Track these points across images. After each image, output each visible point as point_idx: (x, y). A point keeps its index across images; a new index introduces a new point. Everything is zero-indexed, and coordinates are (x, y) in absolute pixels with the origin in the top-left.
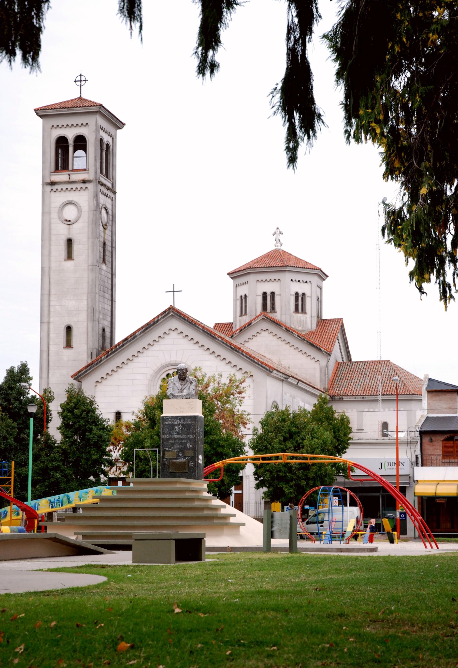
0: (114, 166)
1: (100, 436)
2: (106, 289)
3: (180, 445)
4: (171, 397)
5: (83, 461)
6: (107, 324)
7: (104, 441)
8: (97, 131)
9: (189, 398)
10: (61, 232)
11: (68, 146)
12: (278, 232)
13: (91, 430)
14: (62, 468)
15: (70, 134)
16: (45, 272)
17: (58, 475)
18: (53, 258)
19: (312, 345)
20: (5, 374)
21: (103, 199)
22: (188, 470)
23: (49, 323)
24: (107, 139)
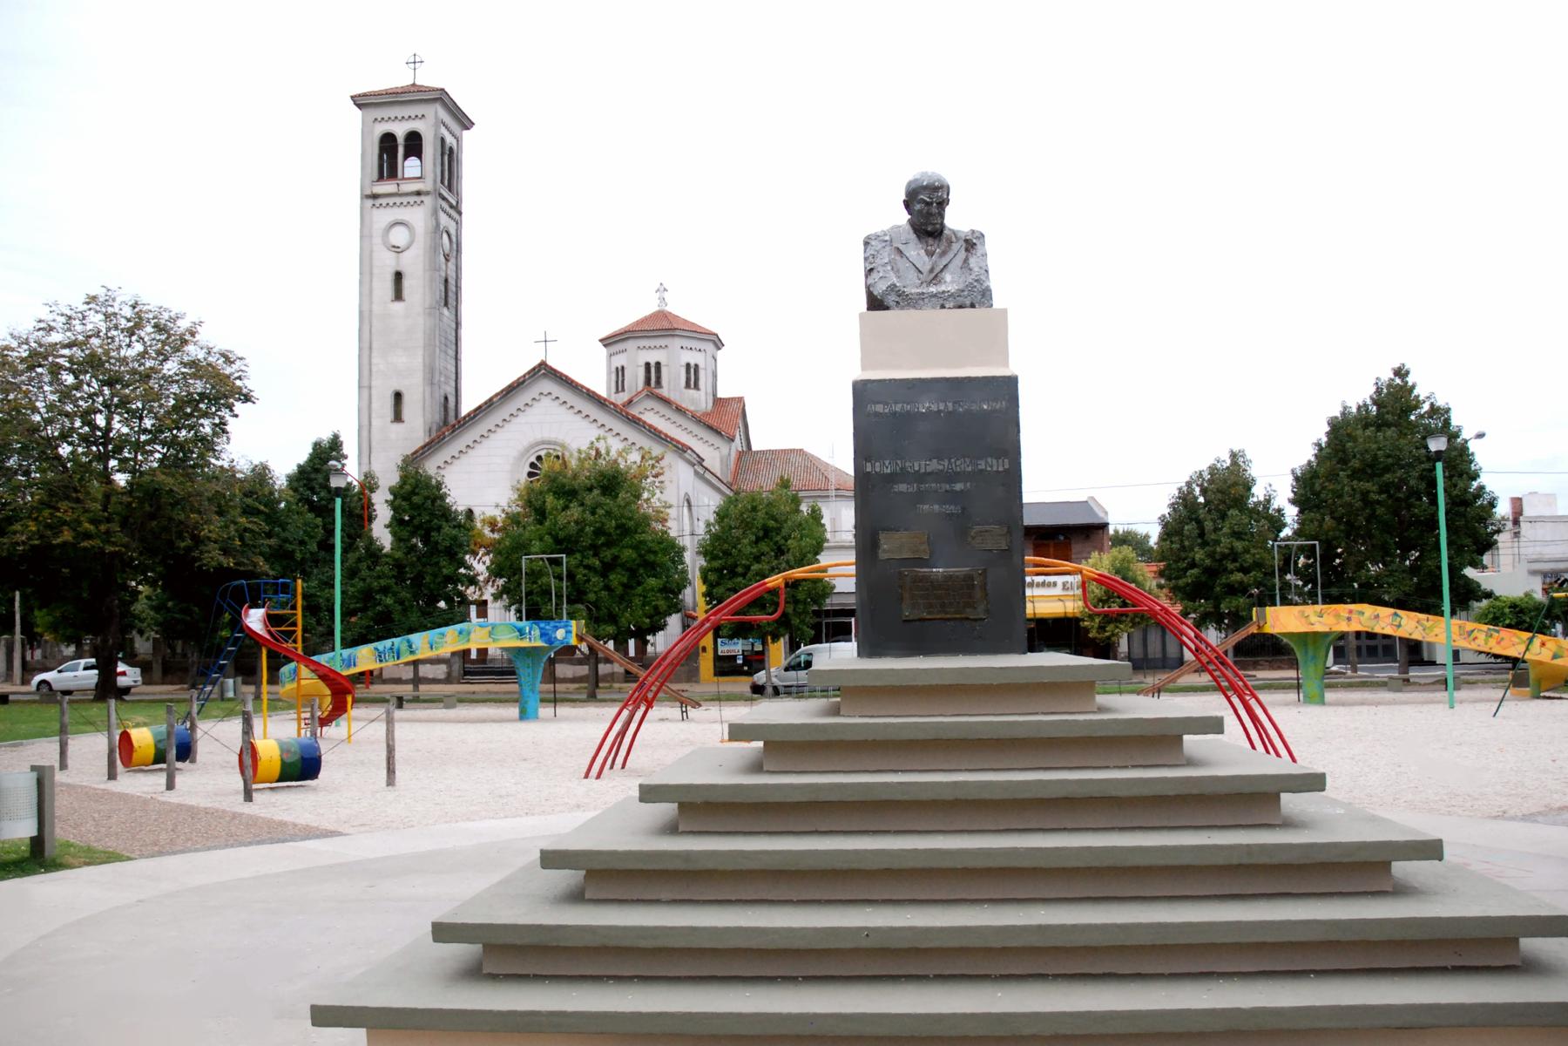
1: (455, 538)
2: (447, 342)
4: (891, 299)
5: (428, 579)
6: (450, 390)
7: (461, 546)
9: (973, 306)
10: (387, 263)
11: (396, 147)
13: (439, 529)
14: (395, 588)
15: (400, 131)
16: (365, 317)
17: (389, 601)
19: (710, 428)
22: (987, 611)
23: (370, 388)
24: (450, 140)
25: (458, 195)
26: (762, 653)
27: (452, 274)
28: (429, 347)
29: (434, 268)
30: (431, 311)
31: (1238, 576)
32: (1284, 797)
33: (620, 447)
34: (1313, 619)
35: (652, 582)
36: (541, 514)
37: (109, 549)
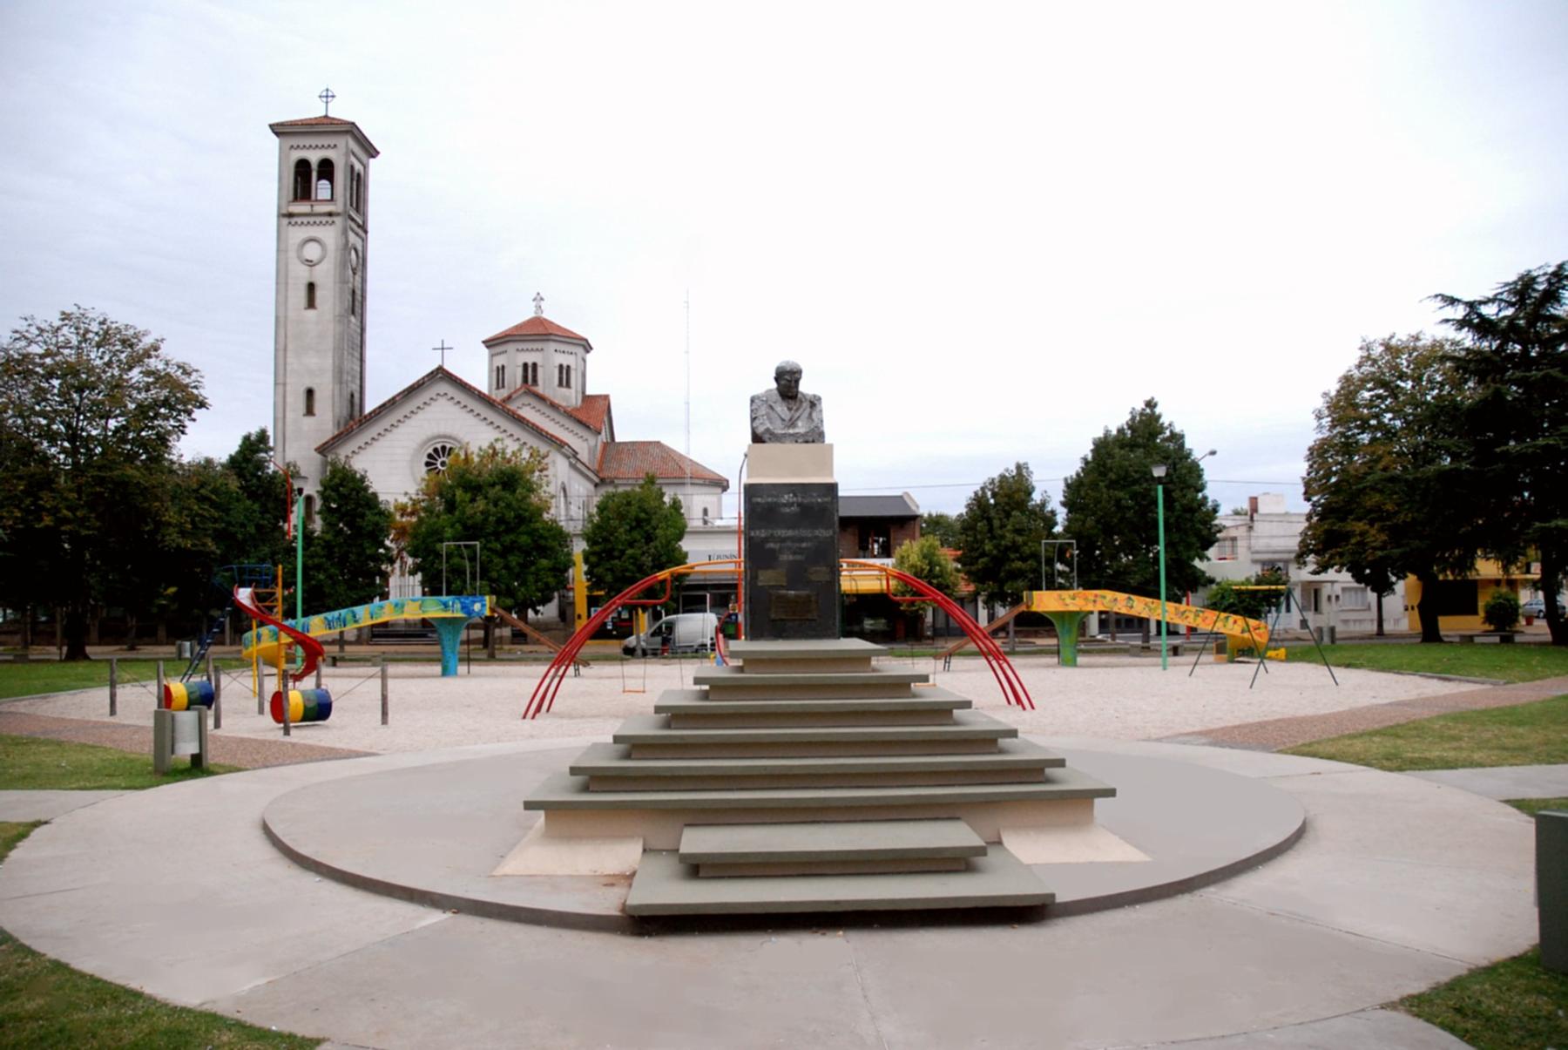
0: (365, 201)
3: (794, 553)
4: (766, 437)
5: (352, 557)
6: (356, 388)
7: (382, 530)
8: (347, 155)
10: (301, 275)
12: (539, 298)
13: (363, 516)
15: (314, 157)
18: (290, 305)
19: (580, 422)
20: (239, 442)
21: (352, 238)
24: (358, 167)
25: (364, 216)
26: (630, 619)
27: (358, 285)
28: (339, 352)
29: (344, 281)
30: (341, 319)
31: (1018, 564)
32: (955, 712)
33: (514, 446)
34: (1068, 601)
35: (544, 562)
36: (451, 506)
37: (84, 532)
